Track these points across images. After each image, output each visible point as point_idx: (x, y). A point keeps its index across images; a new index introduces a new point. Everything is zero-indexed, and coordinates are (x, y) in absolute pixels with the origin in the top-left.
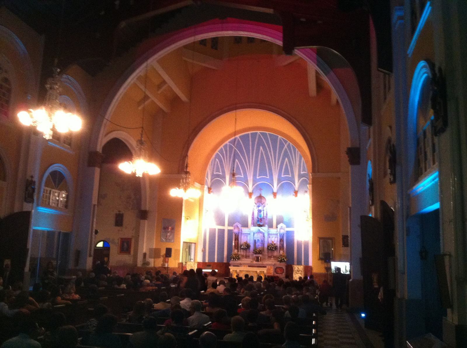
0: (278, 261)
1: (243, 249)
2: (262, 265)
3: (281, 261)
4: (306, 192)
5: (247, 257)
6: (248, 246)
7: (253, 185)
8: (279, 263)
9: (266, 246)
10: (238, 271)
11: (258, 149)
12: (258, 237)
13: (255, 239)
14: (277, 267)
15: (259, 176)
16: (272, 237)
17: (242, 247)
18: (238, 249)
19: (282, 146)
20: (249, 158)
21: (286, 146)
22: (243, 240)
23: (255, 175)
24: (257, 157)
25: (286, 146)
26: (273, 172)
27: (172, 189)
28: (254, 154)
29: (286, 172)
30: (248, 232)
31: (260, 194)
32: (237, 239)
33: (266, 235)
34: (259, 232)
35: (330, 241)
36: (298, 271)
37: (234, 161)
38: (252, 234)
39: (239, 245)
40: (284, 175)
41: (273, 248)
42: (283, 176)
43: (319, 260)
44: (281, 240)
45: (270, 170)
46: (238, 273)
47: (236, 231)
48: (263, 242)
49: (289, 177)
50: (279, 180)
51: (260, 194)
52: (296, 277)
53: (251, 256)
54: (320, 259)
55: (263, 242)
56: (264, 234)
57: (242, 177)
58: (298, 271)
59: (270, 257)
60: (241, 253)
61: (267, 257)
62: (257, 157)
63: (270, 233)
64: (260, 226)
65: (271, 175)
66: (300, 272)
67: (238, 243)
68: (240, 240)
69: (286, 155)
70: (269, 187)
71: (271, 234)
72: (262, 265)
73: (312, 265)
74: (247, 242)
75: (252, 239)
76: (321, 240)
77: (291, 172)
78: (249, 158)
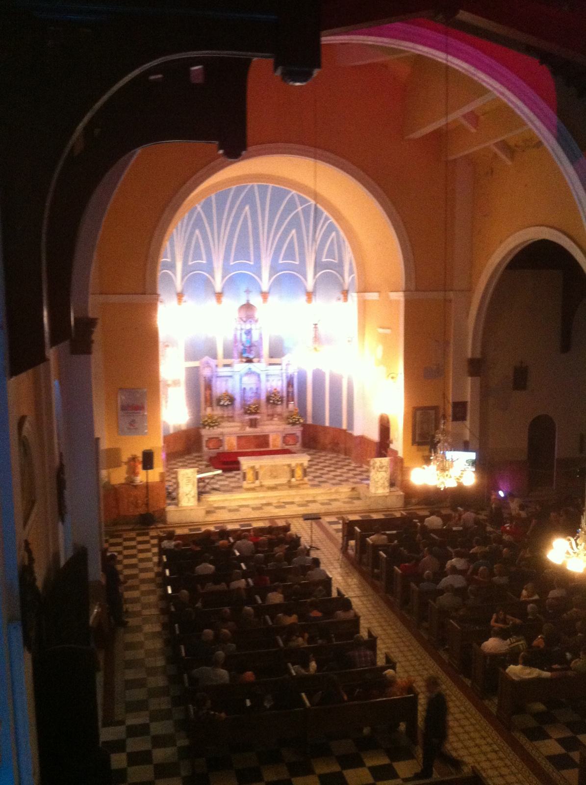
0: (289, 424)
1: (223, 406)
2: (261, 433)
3: (294, 424)
4: (339, 299)
5: (231, 418)
6: (232, 399)
7: (223, 277)
8: (289, 427)
9: (263, 397)
10: (257, 467)
11: (241, 208)
12: (249, 383)
13: (243, 386)
14: (286, 434)
15: (234, 261)
16: (273, 380)
17: (222, 403)
18: (211, 405)
19: (291, 205)
20: (219, 227)
21: (300, 209)
22: (220, 388)
23: (226, 258)
24: (234, 225)
25: (300, 209)
26: (263, 256)
27: (574, 574)
28: (278, 236)
29: (290, 254)
30: (230, 374)
31: (248, 301)
32: (209, 386)
33: (263, 377)
34: (250, 373)
35: (432, 412)
36: (381, 467)
37: (192, 233)
38: (237, 378)
39: (214, 399)
40: (282, 261)
41: (278, 401)
42: (281, 262)
43: (413, 445)
44: (290, 384)
45: (257, 248)
46: (257, 471)
47: (206, 372)
48: (257, 393)
49: (294, 264)
50: (273, 269)
51: (248, 301)
52: (377, 477)
53: (237, 419)
54: (414, 442)
55: (257, 393)
56: (259, 376)
57: (204, 262)
58: (381, 467)
59: (271, 416)
60: (218, 412)
61: (265, 418)
62: (234, 225)
63: (270, 372)
64: (249, 361)
65: (258, 258)
66: (384, 469)
67: (211, 395)
68: (214, 389)
69: (295, 223)
70: (252, 283)
71: (271, 375)
72: (261, 433)
73: (403, 455)
74: (227, 391)
75: (238, 386)
76: (418, 413)
77: (300, 254)
78: (219, 227)
